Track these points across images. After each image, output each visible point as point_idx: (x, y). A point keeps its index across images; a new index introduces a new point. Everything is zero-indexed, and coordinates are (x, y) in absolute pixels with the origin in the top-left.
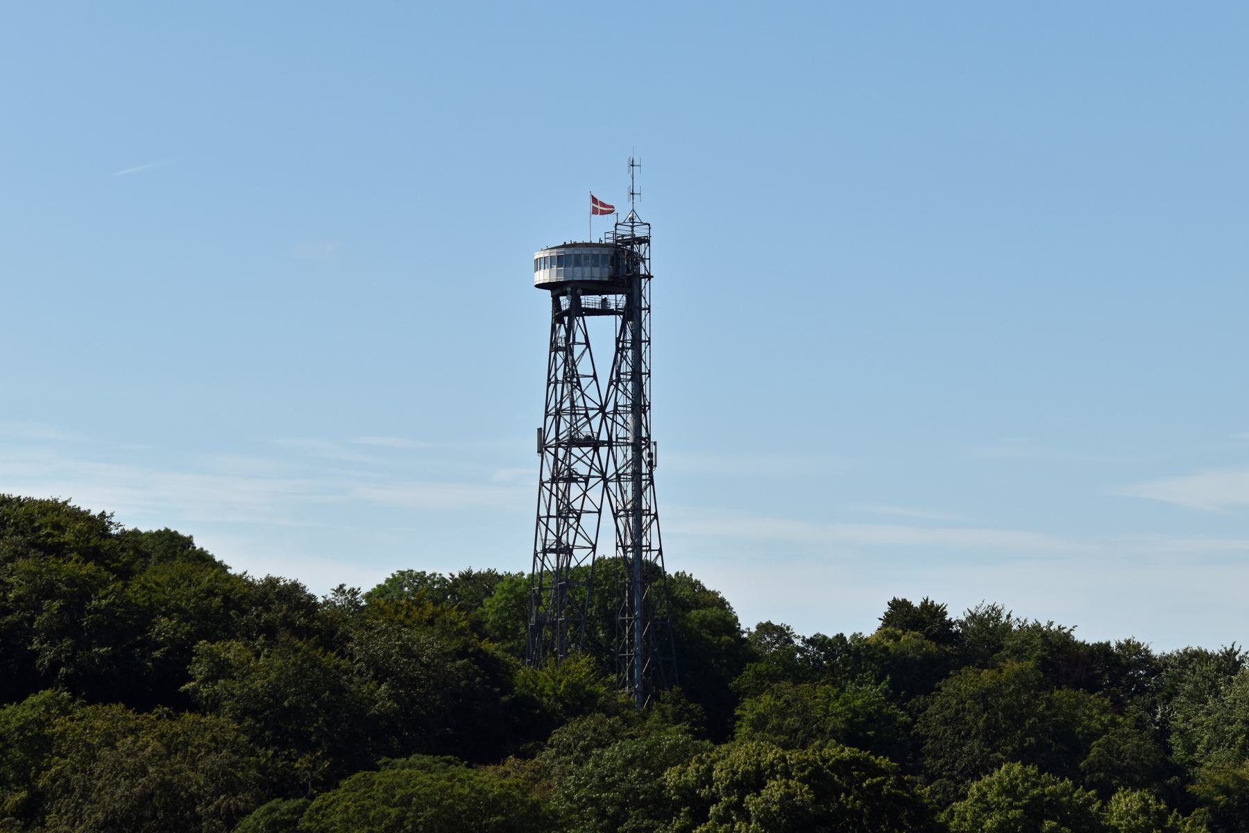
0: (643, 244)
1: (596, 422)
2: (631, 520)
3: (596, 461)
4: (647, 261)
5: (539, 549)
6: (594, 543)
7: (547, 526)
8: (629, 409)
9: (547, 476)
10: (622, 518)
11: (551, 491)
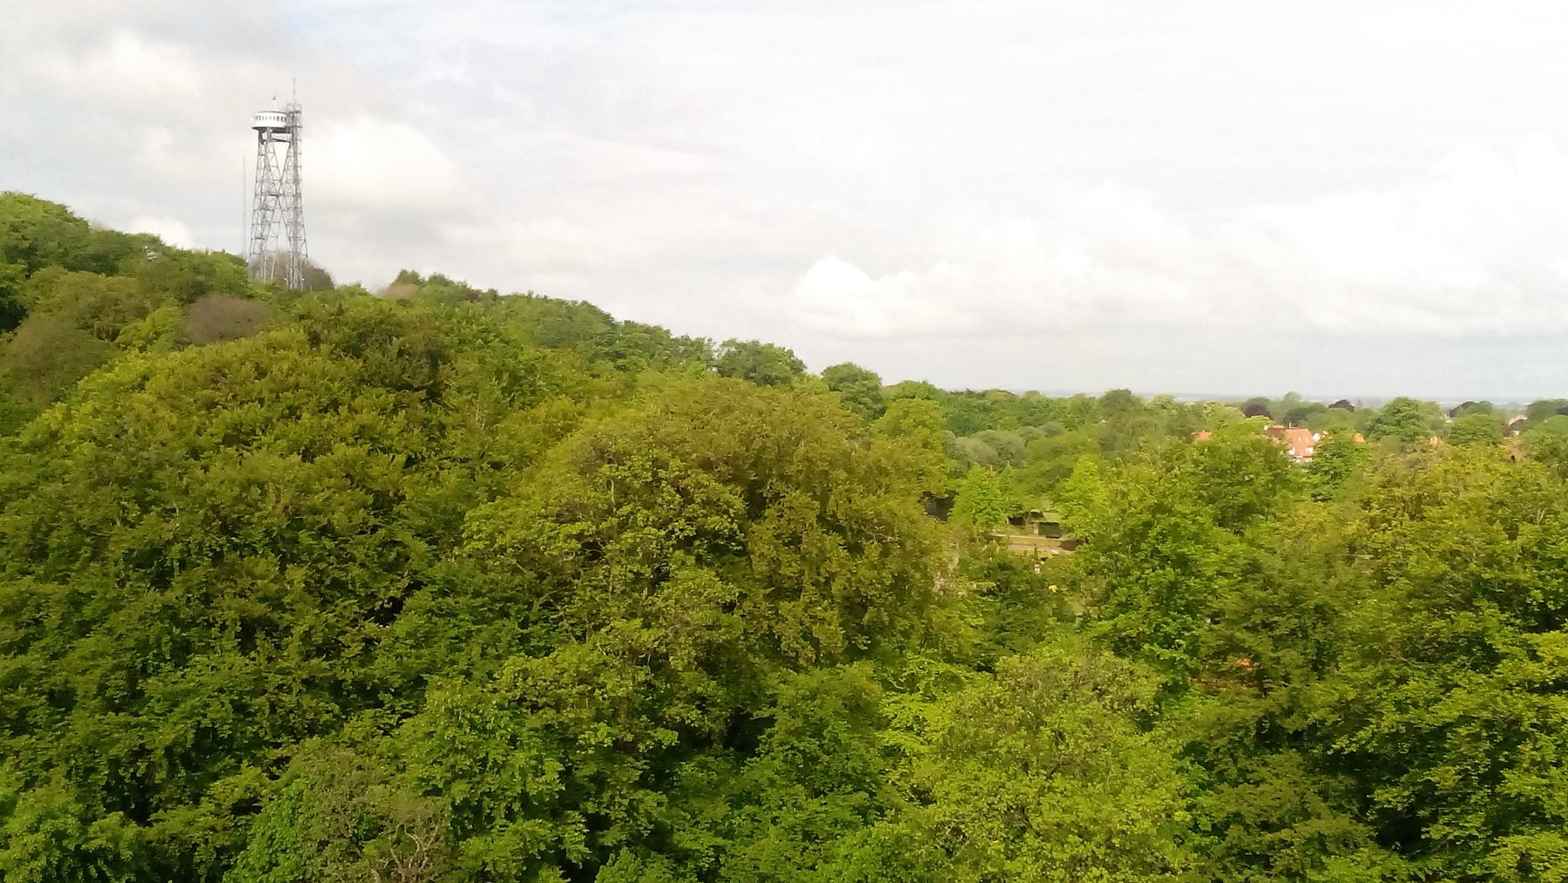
1: (278, 186)
2: (169, 806)
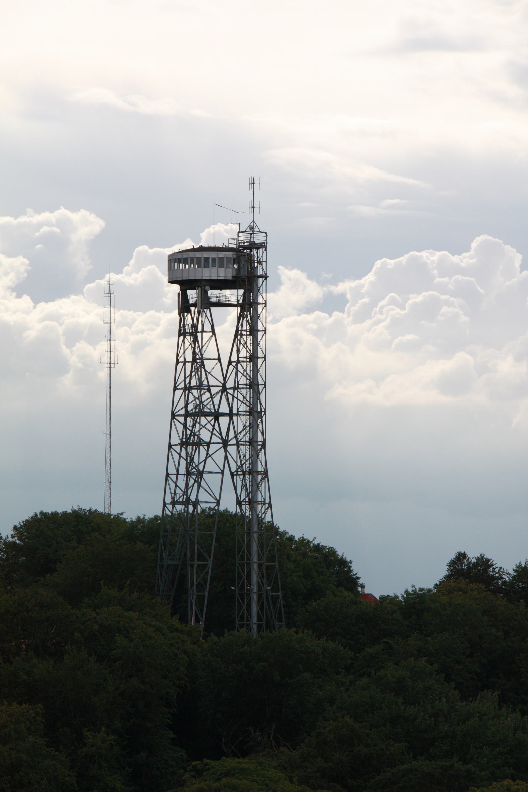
0: (261, 249)
3: (216, 427)
4: (264, 264)
5: (168, 500)
6: (218, 499)
7: (176, 483)
8: (248, 333)
9: (176, 440)
10: (242, 417)
11: (180, 454)
